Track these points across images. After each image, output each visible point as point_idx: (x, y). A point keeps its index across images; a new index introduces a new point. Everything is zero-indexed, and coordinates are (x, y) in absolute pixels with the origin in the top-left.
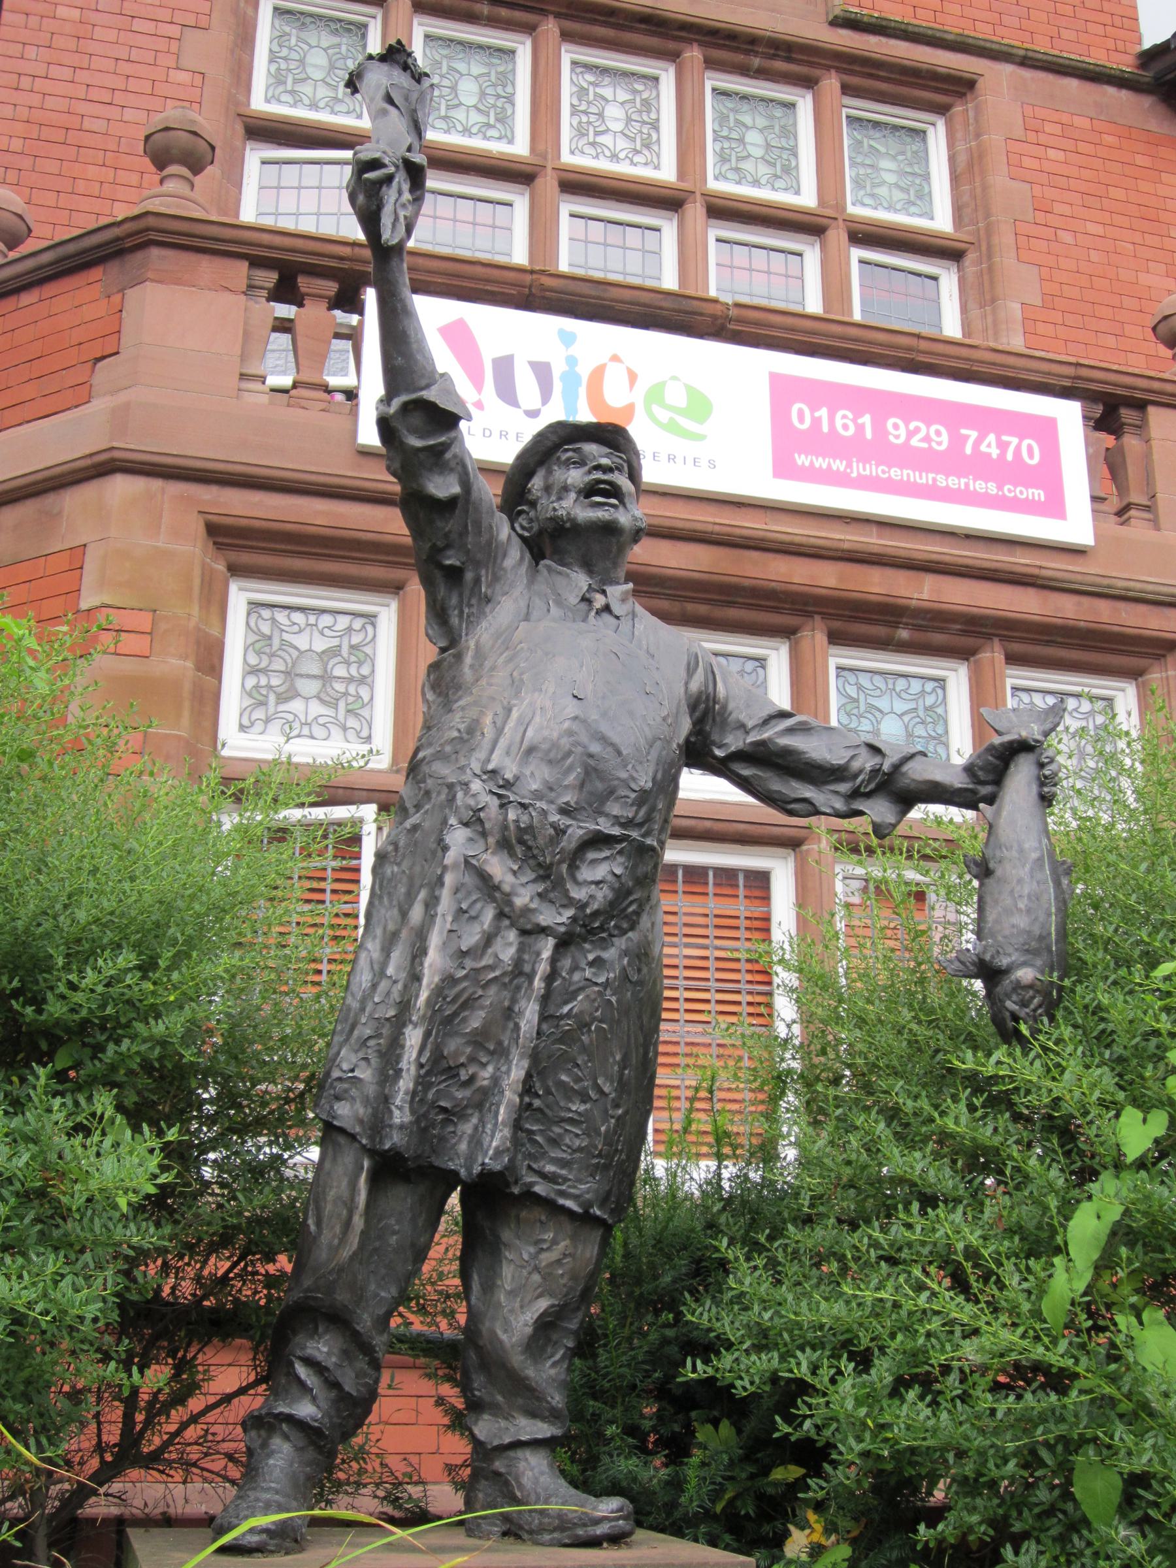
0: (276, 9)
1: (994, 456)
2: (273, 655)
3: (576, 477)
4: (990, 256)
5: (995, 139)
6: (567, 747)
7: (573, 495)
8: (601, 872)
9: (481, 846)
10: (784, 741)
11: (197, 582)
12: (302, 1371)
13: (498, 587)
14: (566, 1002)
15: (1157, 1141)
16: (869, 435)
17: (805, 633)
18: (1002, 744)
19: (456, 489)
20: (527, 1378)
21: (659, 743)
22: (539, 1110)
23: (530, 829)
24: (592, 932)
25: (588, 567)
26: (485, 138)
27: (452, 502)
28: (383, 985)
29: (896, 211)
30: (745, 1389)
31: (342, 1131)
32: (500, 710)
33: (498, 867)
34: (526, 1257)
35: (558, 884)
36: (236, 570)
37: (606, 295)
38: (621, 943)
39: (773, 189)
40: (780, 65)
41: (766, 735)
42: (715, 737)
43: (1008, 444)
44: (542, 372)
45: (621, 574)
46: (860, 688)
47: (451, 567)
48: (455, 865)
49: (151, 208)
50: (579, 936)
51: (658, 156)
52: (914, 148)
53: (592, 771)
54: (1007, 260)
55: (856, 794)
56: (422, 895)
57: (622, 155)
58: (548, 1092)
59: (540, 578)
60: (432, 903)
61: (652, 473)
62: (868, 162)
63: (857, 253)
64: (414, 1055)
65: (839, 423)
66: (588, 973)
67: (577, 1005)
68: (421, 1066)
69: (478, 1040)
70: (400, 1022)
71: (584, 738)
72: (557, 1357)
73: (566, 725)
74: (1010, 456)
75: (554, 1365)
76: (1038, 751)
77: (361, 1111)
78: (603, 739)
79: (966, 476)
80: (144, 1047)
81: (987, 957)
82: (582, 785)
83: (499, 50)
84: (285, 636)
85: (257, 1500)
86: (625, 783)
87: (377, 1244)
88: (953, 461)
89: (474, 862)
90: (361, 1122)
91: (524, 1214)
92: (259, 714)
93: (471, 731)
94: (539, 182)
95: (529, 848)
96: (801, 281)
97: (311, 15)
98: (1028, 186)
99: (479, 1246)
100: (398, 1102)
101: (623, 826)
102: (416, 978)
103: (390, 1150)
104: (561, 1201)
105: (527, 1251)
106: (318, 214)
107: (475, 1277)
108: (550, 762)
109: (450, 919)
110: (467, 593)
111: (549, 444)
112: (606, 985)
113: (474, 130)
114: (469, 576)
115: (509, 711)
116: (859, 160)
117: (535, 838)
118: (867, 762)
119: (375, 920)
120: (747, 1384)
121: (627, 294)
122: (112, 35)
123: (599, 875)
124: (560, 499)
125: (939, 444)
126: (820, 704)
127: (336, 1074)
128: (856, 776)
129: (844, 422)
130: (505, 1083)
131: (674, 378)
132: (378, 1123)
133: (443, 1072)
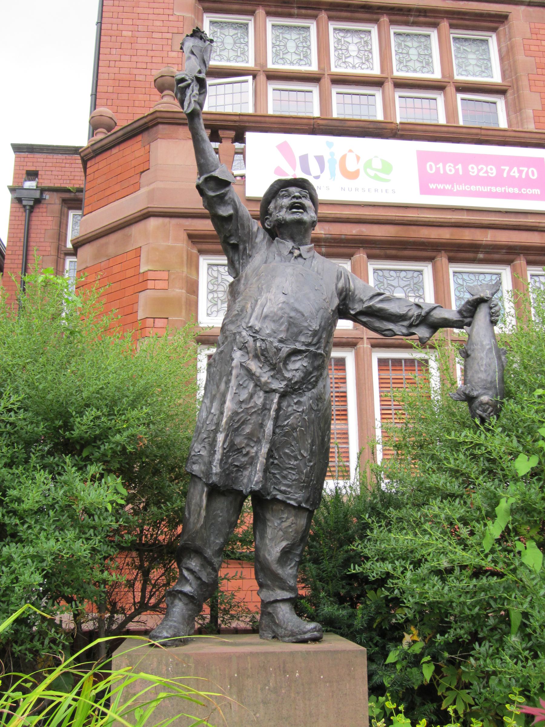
0: (211, 22)
1: (517, 177)
2: (218, 285)
3: (286, 202)
4: (518, 91)
5: (518, 39)
6: (281, 314)
7: (285, 210)
8: (298, 365)
9: (246, 358)
10: (379, 305)
11: (185, 258)
12: (186, 573)
13: (254, 250)
14: (286, 420)
15: (532, 468)
16: (461, 173)
17: (438, 259)
18: (473, 300)
19: (231, 212)
20: (278, 574)
21: (322, 311)
22: (277, 464)
23: (266, 349)
24: (295, 390)
25: (293, 239)
26: (300, 65)
27: (230, 217)
28: (210, 417)
29: (476, 76)
30: (374, 577)
31: (196, 476)
32: (253, 301)
33: (254, 366)
34: (276, 524)
35: (280, 371)
36: (202, 252)
37: (346, 125)
38: (309, 394)
39: (422, 72)
40: (422, 19)
41: (371, 304)
42: (351, 306)
43: (523, 171)
44: (320, 160)
45: (309, 241)
46: (464, 280)
47: (233, 244)
48: (237, 366)
49: (157, 108)
50: (290, 392)
51: (372, 64)
52: (483, 48)
53: (291, 323)
54: (526, 92)
55: (411, 326)
56: (224, 379)
57: (357, 66)
58: (280, 457)
59: (273, 245)
60: (228, 382)
61: (322, 195)
62: (463, 56)
63: (460, 96)
64: (221, 444)
65: (447, 169)
66: (295, 408)
67: (290, 421)
68: (225, 449)
69: (250, 437)
70: (216, 431)
71: (287, 310)
72: (292, 565)
73: (280, 305)
74: (524, 176)
75: (291, 568)
76: (489, 302)
77: (203, 468)
78: (296, 310)
79: (504, 186)
80: (113, 446)
81: (467, 392)
82: (288, 330)
83: (303, 27)
84: (223, 277)
85: (167, 625)
86: (307, 328)
87: (213, 521)
88: (498, 180)
89: (244, 364)
90: (203, 472)
91: (274, 507)
92: (215, 309)
93: (242, 311)
94: (322, 81)
95: (266, 357)
96: (435, 111)
97: (225, 23)
98: (533, 58)
99: (259, 521)
100: (214, 464)
101: (306, 345)
102: (222, 413)
103: (212, 483)
104: (288, 501)
105: (276, 523)
106: (233, 104)
107: (258, 533)
108: (274, 321)
109: (235, 388)
110: (241, 254)
111: (275, 189)
112: (303, 412)
113: (295, 62)
114: (241, 247)
115: (256, 301)
116: (459, 56)
117: (268, 353)
118: (415, 312)
119: (208, 390)
120: (374, 574)
121: (354, 124)
122: (145, 41)
123: (296, 368)
124: (280, 212)
125: (492, 174)
126: (446, 288)
127: (193, 453)
128: (411, 318)
129: (450, 169)
130: (259, 454)
131: (376, 157)
132: (208, 473)
133: (235, 451)
